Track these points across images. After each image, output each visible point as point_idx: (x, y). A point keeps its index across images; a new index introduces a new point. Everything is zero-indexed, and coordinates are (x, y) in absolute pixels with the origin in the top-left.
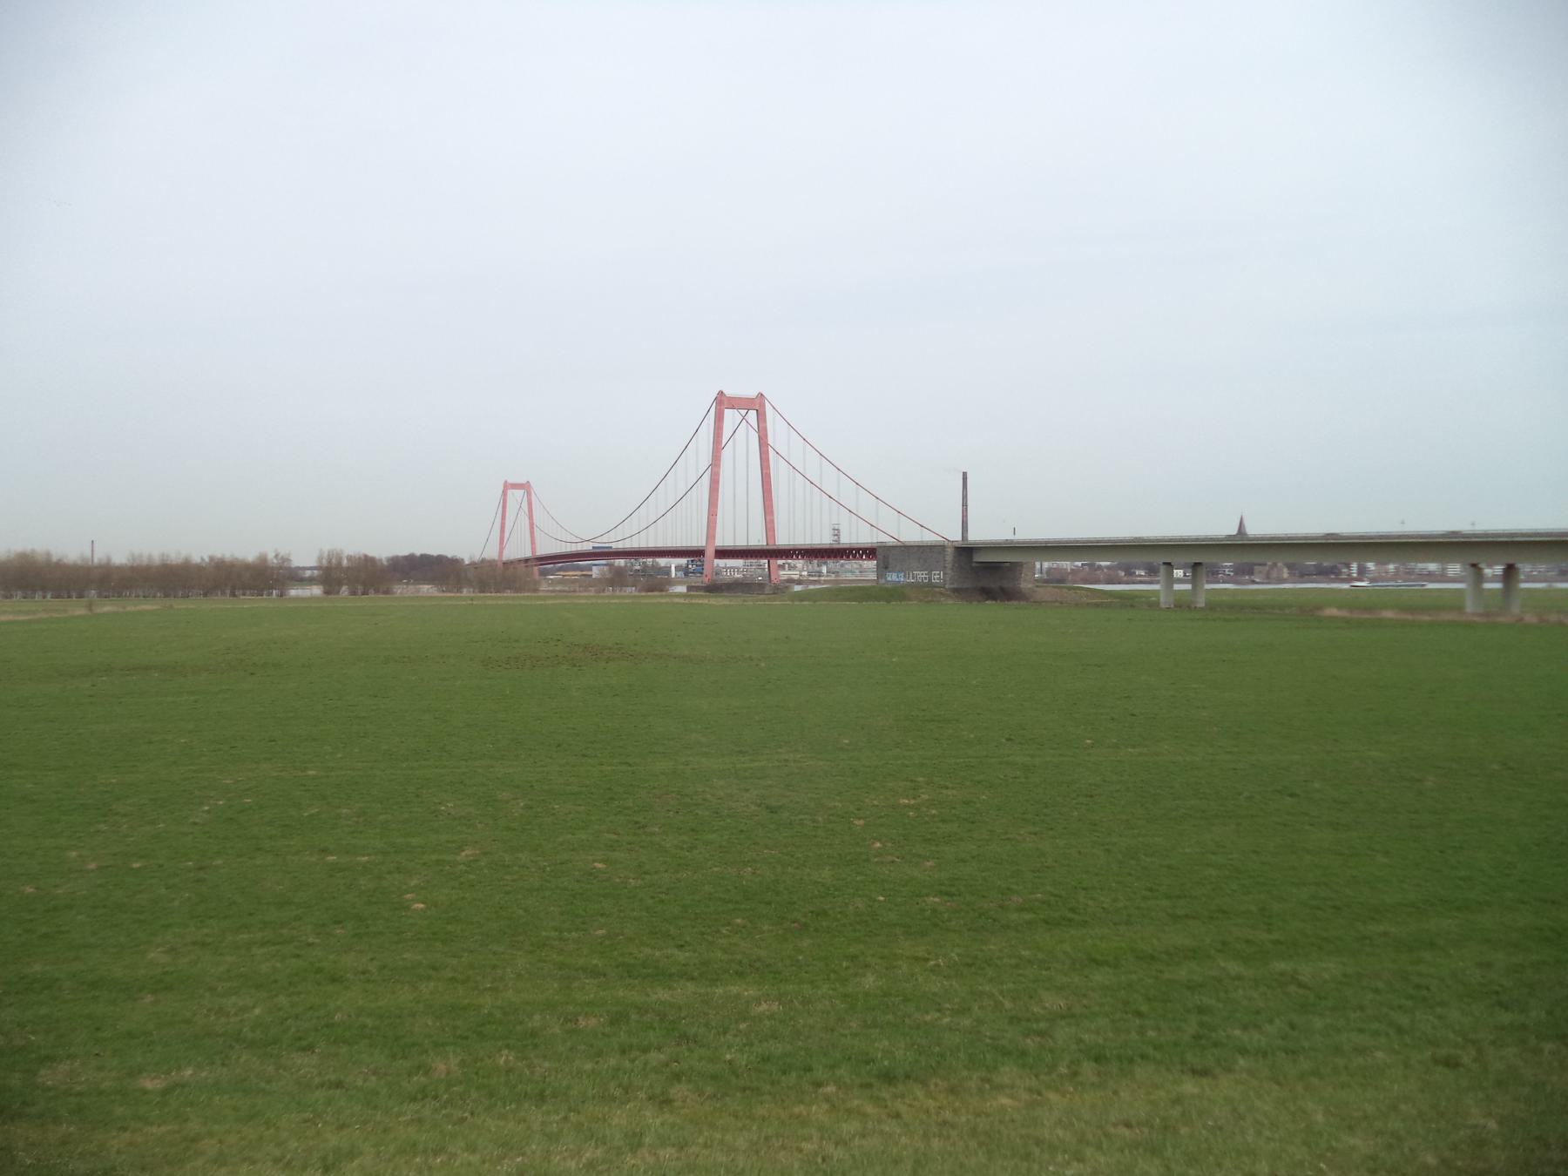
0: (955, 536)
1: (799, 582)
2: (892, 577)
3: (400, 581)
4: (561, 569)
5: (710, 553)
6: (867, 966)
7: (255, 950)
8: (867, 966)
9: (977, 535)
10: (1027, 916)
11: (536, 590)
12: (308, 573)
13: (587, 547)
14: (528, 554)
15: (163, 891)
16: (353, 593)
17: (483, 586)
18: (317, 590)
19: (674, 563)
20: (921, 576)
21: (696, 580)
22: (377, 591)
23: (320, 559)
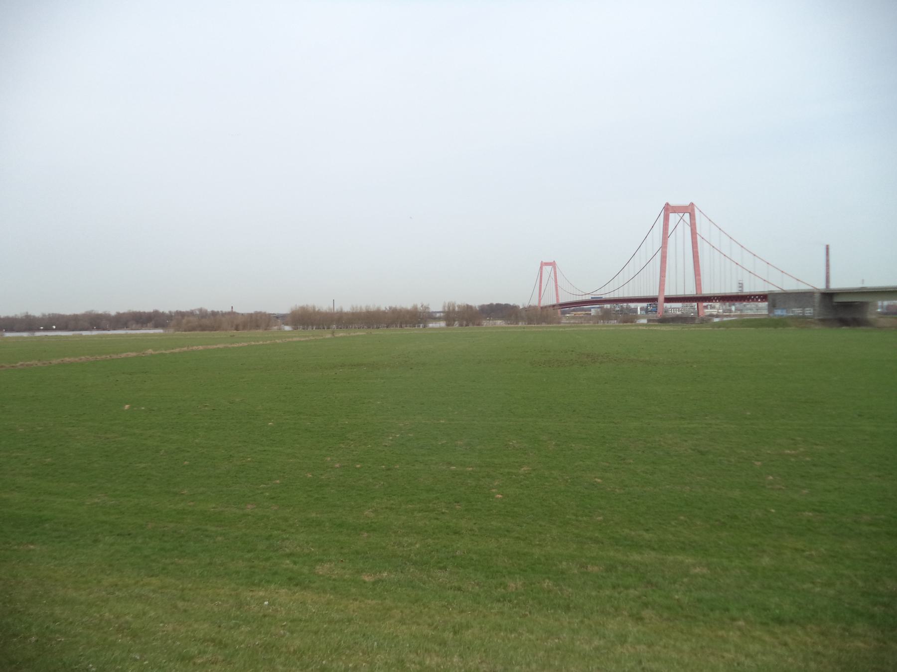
0: (821, 286)
1: (717, 316)
2: (779, 312)
3: (485, 318)
4: (574, 311)
5: (661, 299)
6: (764, 551)
7: (416, 514)
8: (764, 551)
9: (835, 285)
10: (874, 529)
11: (559, 323)
12: (438, 315)
13: (588, 298)
14: (555, 302)
15: (371, 480)
16: (461, 325)
17: (530, 321)
18: (442, 324)
19: (639, 306)
20: (797, 311)
21: (652, 316)
22: (474, 324)
23: (444, 307)
